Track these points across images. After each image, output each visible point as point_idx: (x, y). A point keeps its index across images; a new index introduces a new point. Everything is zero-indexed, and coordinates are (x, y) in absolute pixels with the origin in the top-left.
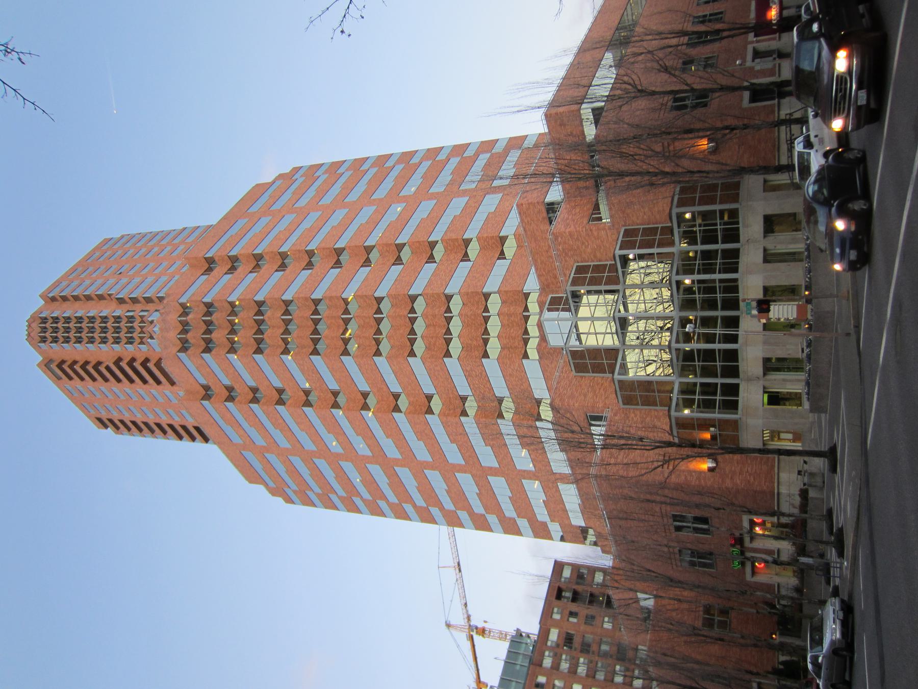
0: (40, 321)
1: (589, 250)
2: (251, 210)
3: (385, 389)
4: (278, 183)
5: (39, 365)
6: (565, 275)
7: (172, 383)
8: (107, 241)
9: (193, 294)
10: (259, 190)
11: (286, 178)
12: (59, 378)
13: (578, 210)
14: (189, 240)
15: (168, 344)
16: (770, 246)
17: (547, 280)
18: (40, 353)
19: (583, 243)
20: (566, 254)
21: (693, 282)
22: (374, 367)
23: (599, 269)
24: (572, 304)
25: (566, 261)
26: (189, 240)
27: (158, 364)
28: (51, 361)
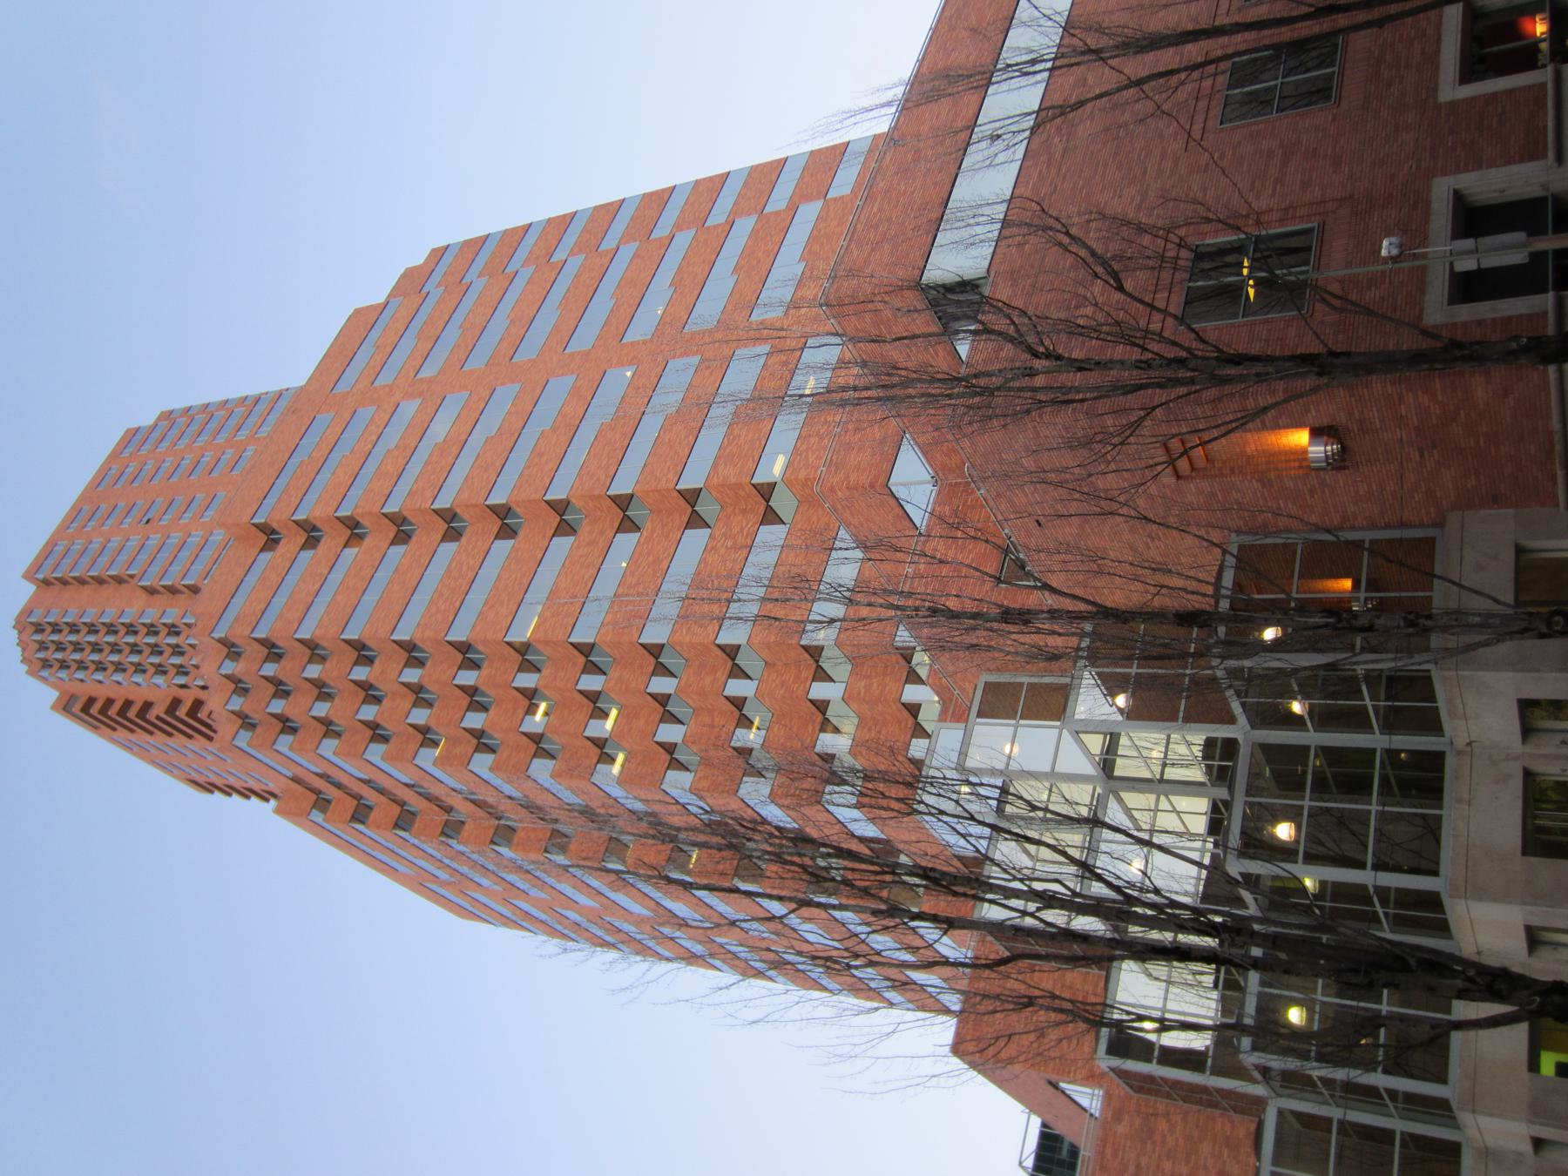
0: (33, 629)
2: (342, 388)
4: (395, 302)
5: (54, 707)
8: (131, 434)
9: (237, 619)
10: (362, 322)
11: (412, 283)
12: (96, 728)
14: (264, 432)
15: (296, 632)
16: (1539, 767)
18: (54, 686)
21: (1323, 884)
26: (264, 432)
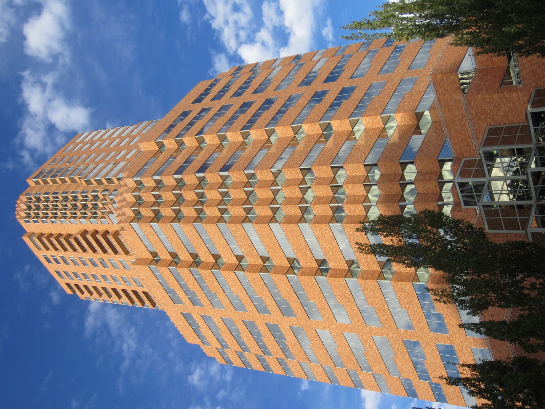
1: (501, 113)
3: (309, 254)
6: (478, 139)
7: (127, 253)
13: (489, 77)
17: (460, 148)
19: (495, 106)
20: (479, 118)
22: (299, 233)
23: (510, 130)
24: (486, 169)
25: (479, 125)
27: (116, 235)
28: (86, 232)
